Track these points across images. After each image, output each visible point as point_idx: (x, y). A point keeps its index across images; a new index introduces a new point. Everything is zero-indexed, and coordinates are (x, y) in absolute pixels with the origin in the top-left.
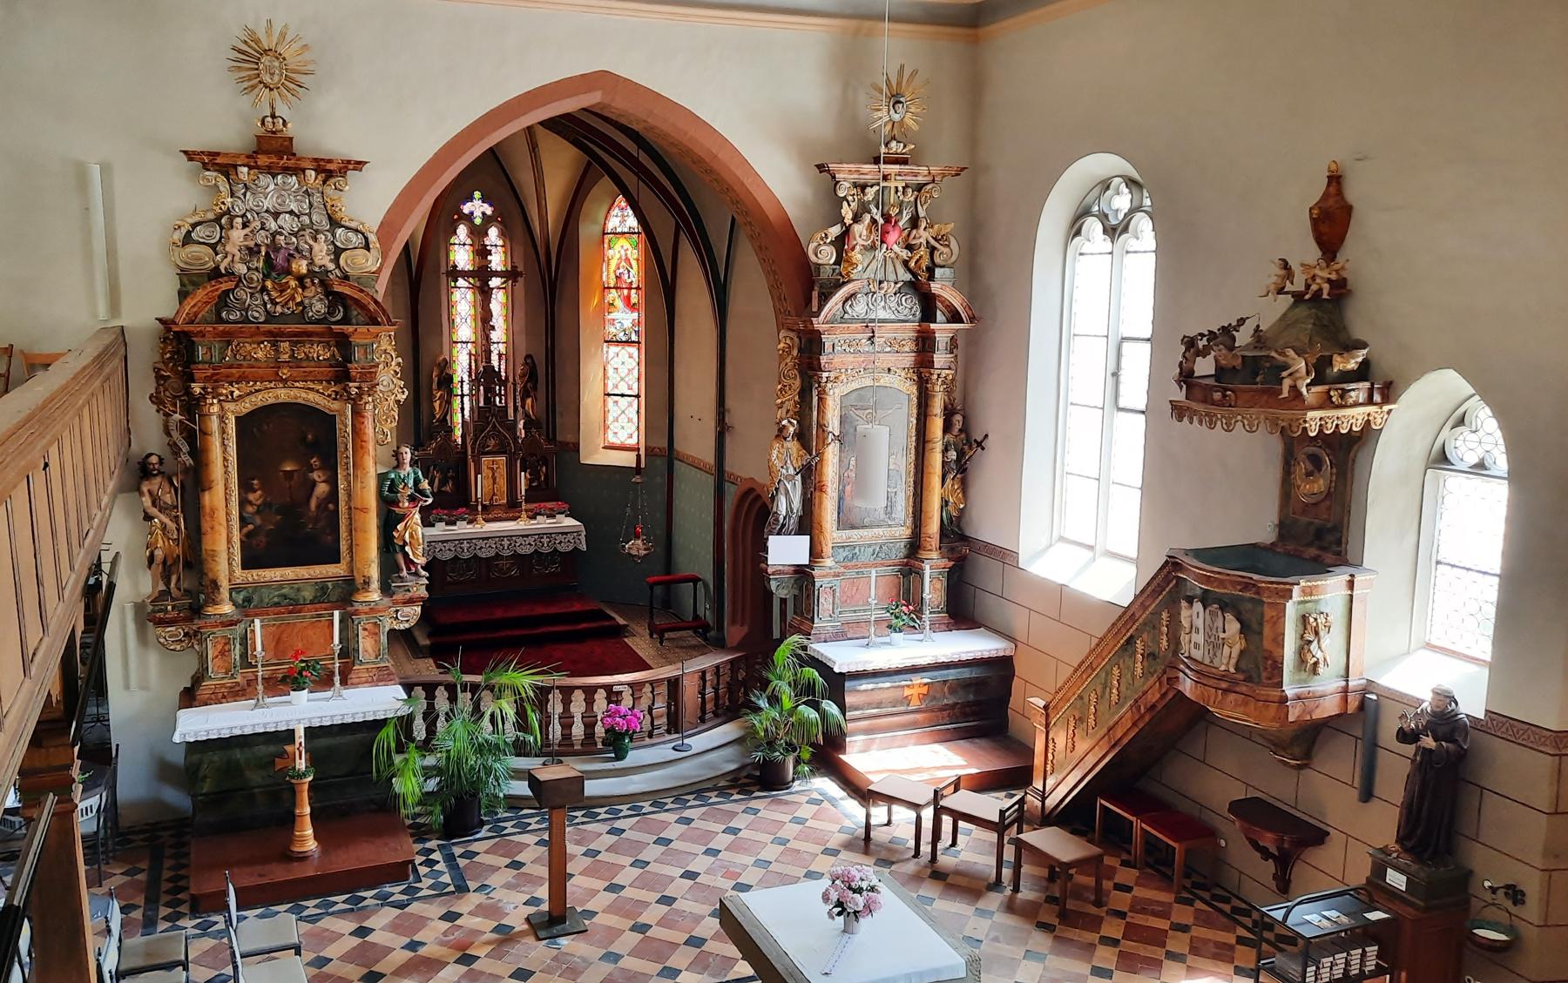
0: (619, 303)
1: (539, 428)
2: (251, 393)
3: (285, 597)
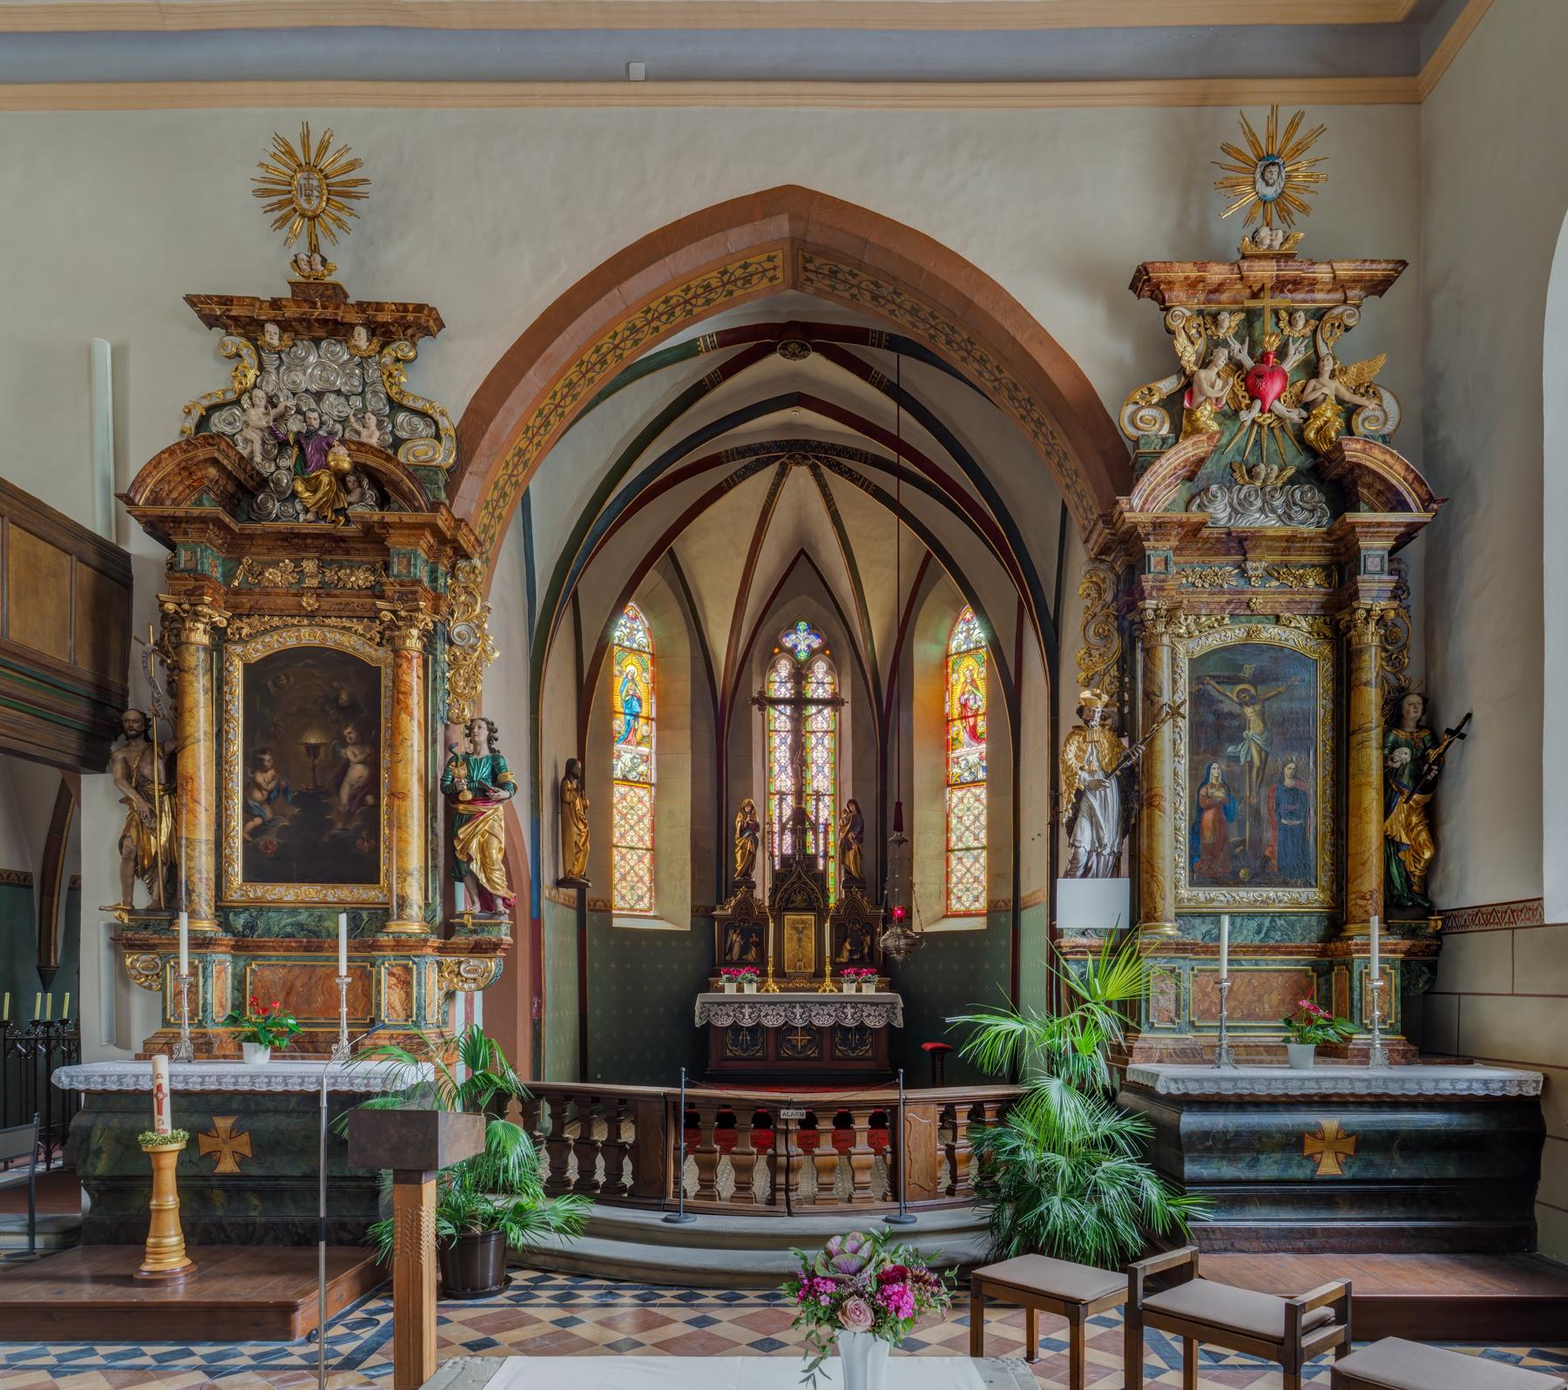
0: (964, 736)
1: (863, 888)
2: (265, 632)
3: (301, 926)
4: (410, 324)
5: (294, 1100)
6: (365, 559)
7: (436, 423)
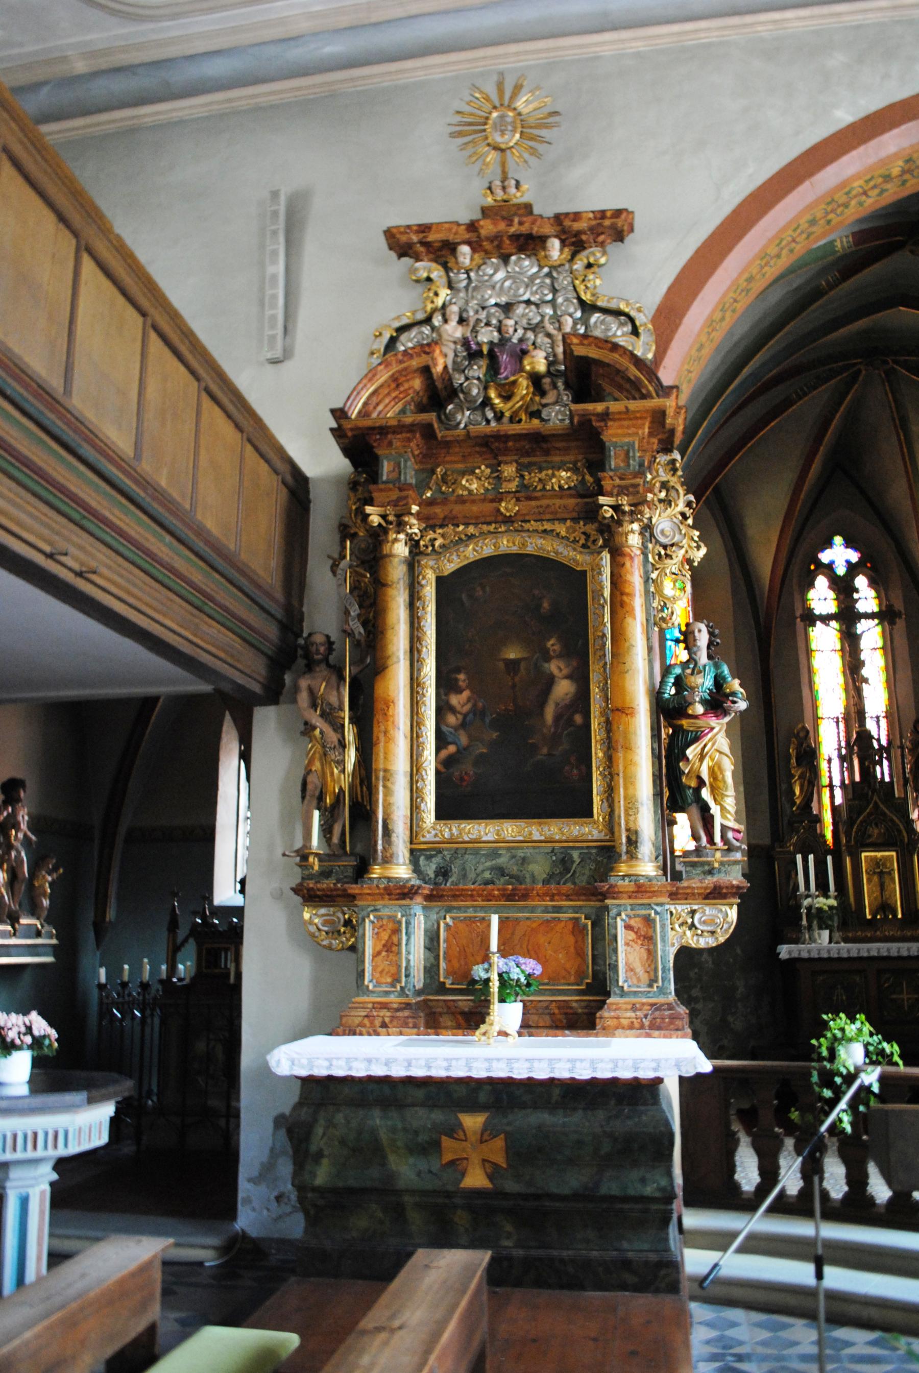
4: (613, 227)
5: (557, 1092)
6: (567, 458)
7: (632, 320)
